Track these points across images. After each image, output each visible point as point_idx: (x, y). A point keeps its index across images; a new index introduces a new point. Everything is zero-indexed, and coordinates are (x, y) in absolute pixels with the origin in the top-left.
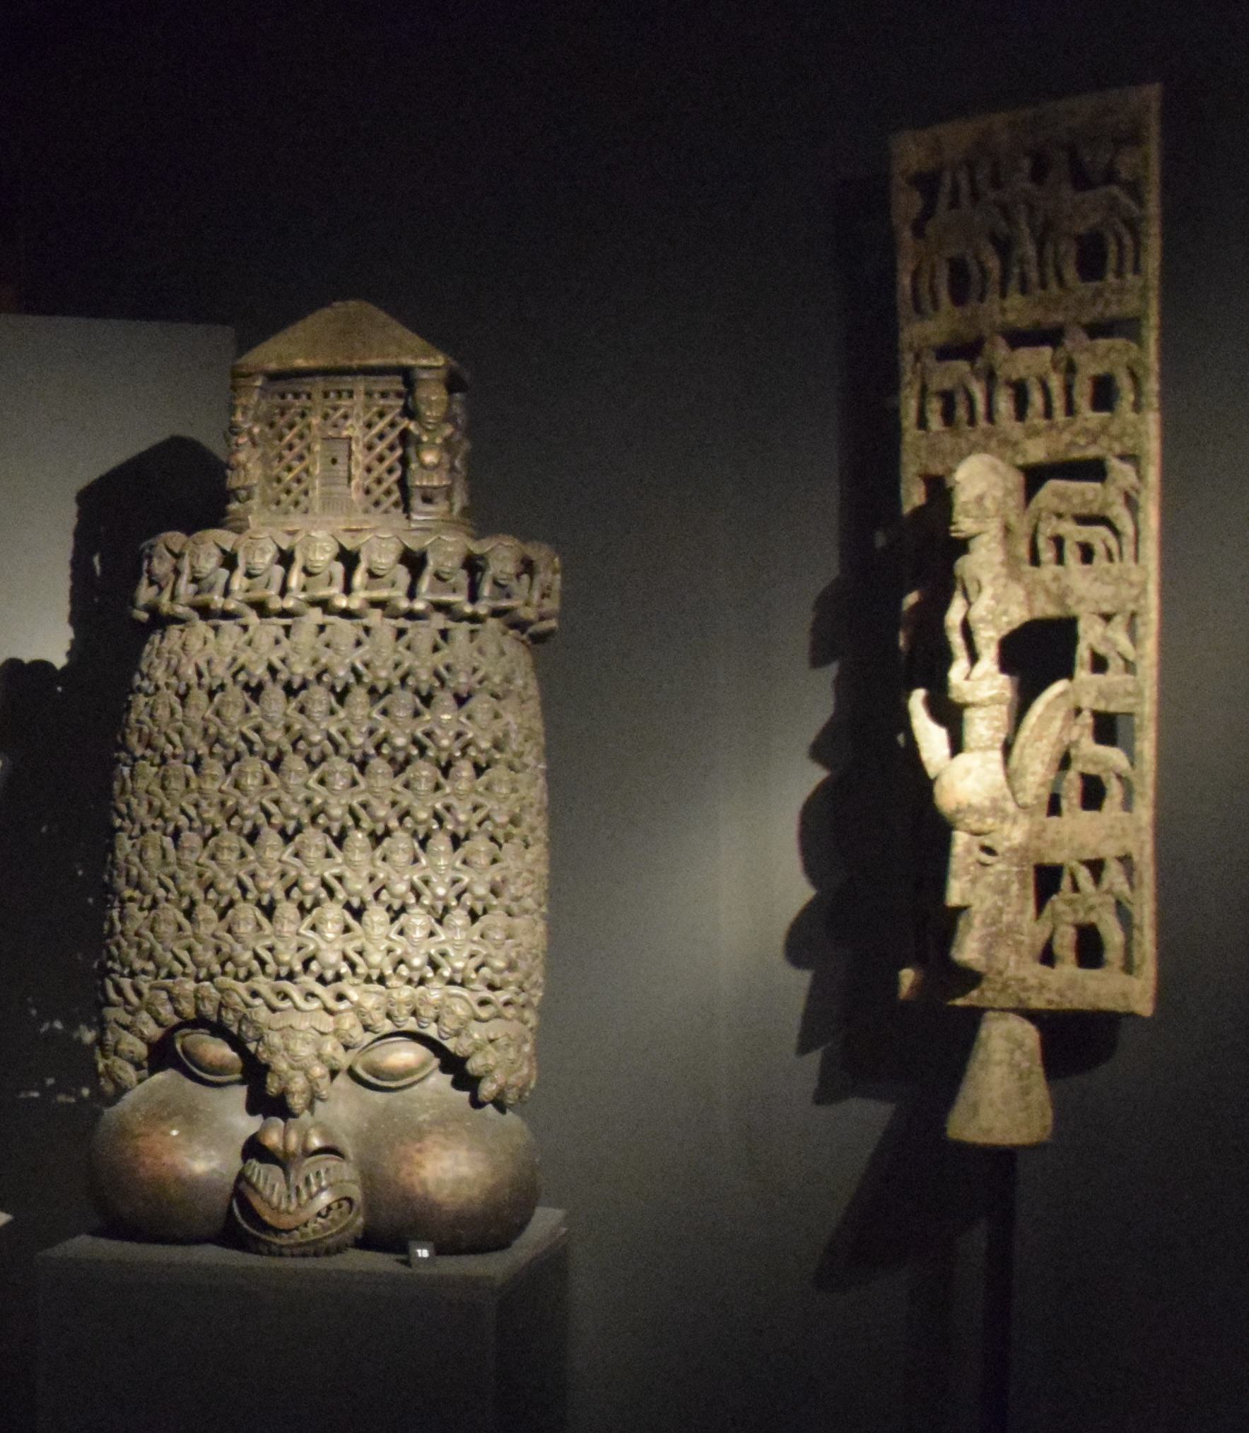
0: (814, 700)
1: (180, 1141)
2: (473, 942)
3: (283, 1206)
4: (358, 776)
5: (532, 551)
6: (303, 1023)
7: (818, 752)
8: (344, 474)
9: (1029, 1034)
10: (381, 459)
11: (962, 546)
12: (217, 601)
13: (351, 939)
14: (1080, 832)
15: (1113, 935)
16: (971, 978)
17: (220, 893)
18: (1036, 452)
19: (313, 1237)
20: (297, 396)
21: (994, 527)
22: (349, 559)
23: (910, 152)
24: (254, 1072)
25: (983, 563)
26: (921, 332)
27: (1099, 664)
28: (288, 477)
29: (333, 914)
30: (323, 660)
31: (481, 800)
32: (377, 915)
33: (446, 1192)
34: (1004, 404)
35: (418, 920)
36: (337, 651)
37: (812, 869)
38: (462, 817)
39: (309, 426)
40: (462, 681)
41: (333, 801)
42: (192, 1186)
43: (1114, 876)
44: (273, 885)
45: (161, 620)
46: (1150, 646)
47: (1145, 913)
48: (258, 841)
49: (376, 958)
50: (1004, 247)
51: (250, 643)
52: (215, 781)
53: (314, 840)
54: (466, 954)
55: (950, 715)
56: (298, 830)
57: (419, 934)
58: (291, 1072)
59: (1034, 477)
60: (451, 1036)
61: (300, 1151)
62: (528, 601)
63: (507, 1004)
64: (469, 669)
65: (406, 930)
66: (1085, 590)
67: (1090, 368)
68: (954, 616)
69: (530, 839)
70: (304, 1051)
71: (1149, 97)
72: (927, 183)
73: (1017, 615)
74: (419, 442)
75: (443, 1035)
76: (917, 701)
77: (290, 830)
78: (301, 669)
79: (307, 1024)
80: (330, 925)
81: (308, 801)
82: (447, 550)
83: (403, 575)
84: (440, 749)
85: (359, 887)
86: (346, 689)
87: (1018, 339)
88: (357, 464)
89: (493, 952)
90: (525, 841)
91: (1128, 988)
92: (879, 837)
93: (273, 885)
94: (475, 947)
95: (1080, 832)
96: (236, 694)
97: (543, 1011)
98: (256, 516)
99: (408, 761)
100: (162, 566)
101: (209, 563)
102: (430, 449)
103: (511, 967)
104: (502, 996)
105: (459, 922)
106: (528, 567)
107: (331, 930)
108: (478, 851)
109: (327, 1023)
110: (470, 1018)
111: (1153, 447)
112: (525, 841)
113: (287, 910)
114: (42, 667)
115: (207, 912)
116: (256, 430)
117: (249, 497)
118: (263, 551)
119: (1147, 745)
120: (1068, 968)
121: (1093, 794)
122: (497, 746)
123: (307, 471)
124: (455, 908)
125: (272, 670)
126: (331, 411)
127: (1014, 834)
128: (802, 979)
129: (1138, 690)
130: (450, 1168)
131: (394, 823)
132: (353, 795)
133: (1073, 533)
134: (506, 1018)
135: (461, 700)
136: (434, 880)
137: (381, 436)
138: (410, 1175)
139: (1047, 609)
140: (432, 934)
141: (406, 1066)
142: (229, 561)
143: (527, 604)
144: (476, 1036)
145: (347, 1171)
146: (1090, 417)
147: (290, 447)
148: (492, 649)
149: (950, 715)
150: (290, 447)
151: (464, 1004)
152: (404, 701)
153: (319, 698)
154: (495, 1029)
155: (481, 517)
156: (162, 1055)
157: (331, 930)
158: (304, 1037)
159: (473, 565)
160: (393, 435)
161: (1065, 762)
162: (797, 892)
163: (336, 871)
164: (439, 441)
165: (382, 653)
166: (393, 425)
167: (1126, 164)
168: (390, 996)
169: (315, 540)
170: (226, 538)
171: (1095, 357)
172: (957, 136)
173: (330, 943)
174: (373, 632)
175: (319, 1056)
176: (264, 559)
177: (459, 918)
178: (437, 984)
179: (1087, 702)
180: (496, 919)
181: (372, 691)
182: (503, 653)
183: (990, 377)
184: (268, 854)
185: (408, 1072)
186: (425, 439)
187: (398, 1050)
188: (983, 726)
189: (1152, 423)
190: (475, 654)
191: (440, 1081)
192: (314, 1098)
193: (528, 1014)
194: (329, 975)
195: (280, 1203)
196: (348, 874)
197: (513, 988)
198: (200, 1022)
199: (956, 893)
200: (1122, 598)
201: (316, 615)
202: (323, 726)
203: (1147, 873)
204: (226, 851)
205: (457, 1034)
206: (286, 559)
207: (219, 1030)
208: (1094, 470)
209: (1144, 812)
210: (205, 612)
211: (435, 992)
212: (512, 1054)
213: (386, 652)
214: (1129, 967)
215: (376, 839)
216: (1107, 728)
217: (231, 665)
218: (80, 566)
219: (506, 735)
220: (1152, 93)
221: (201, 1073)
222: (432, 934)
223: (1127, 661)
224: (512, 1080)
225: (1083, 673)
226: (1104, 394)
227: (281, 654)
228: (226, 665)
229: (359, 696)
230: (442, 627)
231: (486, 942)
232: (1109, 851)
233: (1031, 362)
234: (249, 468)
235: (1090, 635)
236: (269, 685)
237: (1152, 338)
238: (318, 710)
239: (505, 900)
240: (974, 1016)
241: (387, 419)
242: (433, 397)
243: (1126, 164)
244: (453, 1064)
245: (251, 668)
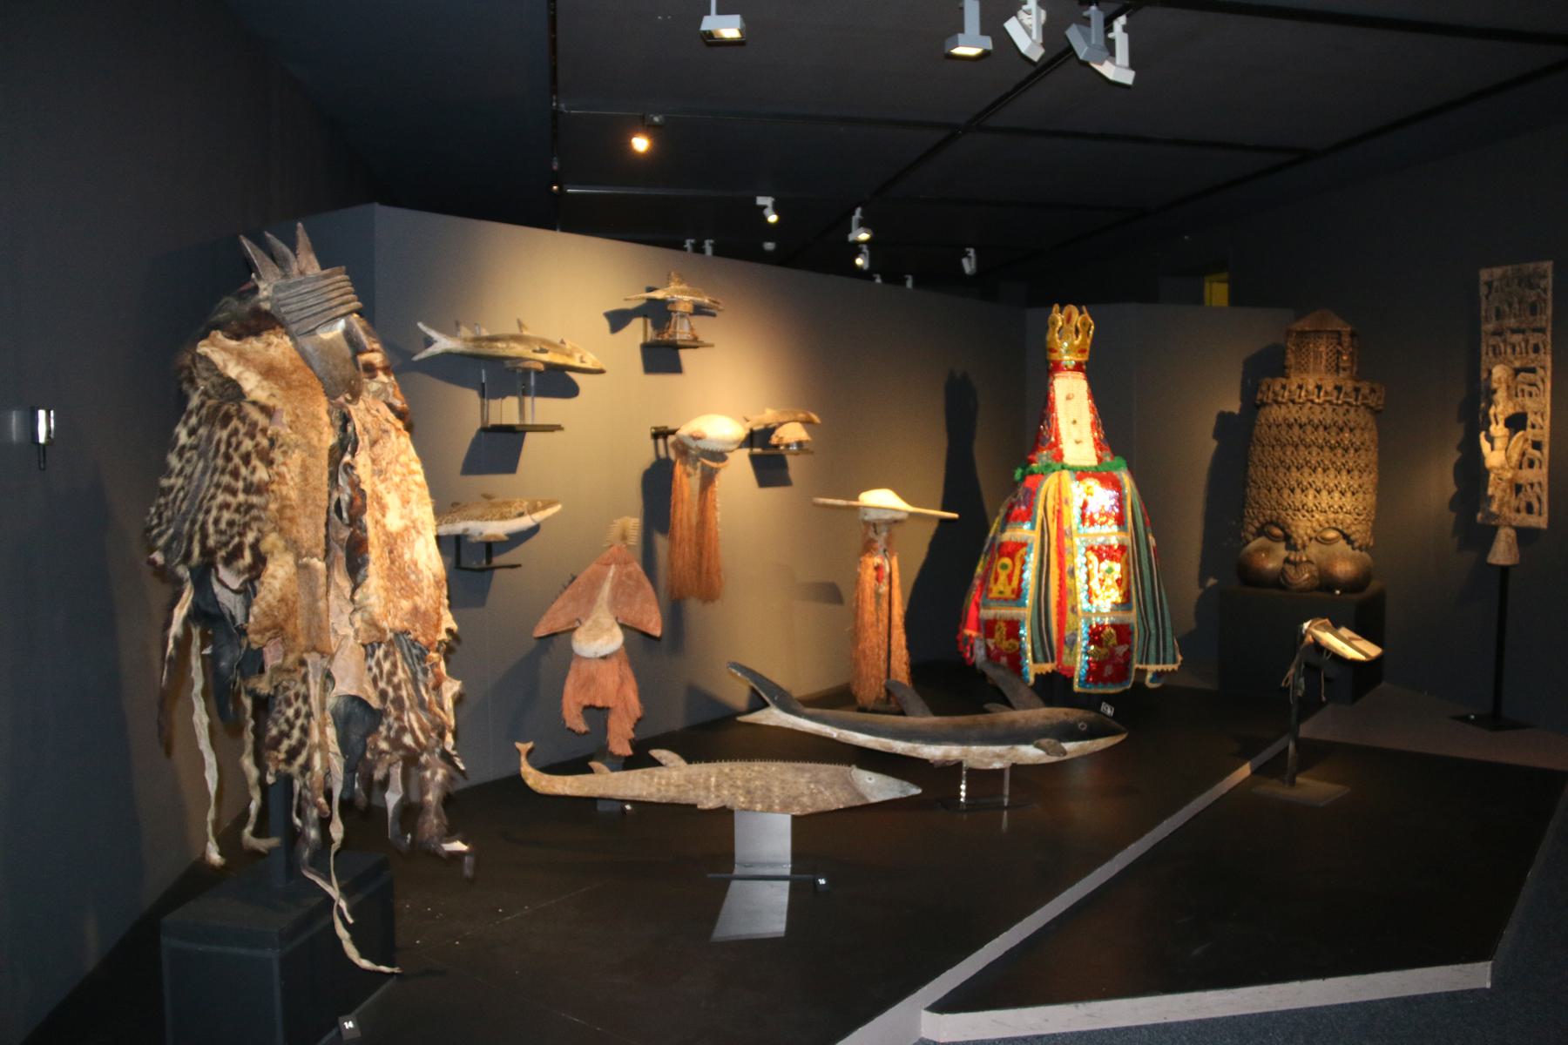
0: (1458, 433)
5: (1376, 386)
7: (1459, 448)
9: (1512, 533)
11: (1495, 392)
14: (1527, 475)
15: (1536, 505)
16: (1497, 517)
18: (1517, 364)
21: (1504, 386)
22: (1319, 388)
23: (1484, 275)
24: (1287, 538)
25: (1501, 396)
26: (1489, 327)
27: (1533, 426)
29: (1311, 493)
32: (1324, 493)
34: (1509, 350)
37: (1457, 483)
40: (1352, 424)
42: (1272, 571)
43: (1536, 488)
44: (1293, 483)
45: (1264, 404)
46: (1547, 422)
47: (1545, 499)
50: (1510, 305)
52: (1278, 452)
53: (1306, 470)
55: (1491, 439)
59: (1517, 372)
62: (1371, 401)
66: (1530, 404)
67: (1532, 342)
68: (1492, 411)
70: (1301, 532)
71: (1548, 266)
72: (1489, 284)
73: (1510, 411)
76: (1482, 435)
78: (1304, 420)
82: (1349, 386)
83: (1335, 393)
87: (1514, 331)
91: (1540, 521)
92: (1472, 471)
93: (1293, 483)
95: (1527, 475)
96: (1284, 427)
97: (1374, 522)
98: (1292, 373)
100: (1264, 388)
101: (1278, 388)
106: (1373, 391)
111: (1549, 365)
113: (1298, 491)
114: (1231, 414)
115: (1274, 491)
119: (1546, 450)
120: (1524, 514)
121: (1531, 464)
127: (1509, 475)
128: (1453, 515)
129: (1544, 435)
130: (1344, 568)
133: (1527, 388)
139: (1519, 410)
142: (1284, 387)
145: (1314, 568)
146: (1532, 356)
149: (1491, 439)
152: (1334, 431)
153: (1309, 429)
154: (1359, 527)
155: (1358, 377)
156: (1260, 532)
158: (1303, 527)
159: (1357, 390)
161: (1523, 454)
162: (1452, 489)
165: (1328, 416)
167: (1543, 284)
170: (1284, 381)
171: (1534, 339)
172: (1498, 272)
173: (1310, 500)
176: (1294, 387)
179: (1530, 437)
180: (1360, 495)
183: (1505, 341)
188: (1499, 444)
189: (1548, 359)
191: (1342, 542)
192: (1304, 547)
198: (1271, 523)
199: (1490, 491)
200: (1539, 407)
203: (1546, 487)
206: (1300, 387)
207: (1277, 525)
208: (1533, 371)
209: (1545, 470)
210: (1276, 402)
211: (1341, 516)
214: (1540, 514)
215: (1324, 471)
216: (1537, 445)
218: (1244, 383)
220: (1548, 266)
221: (1275, 538)
223: (1541, 425)
225: (1529, 429)
226: (1536, 349)
232: (1535, 481)
233: (1517, 338)
234: (1291, 359)
235: (1531, 418)
237: (1549, 334)
240: (1495, 529)
242: (1346, 340)
243: (1543, 284)
244: (1346, 537)
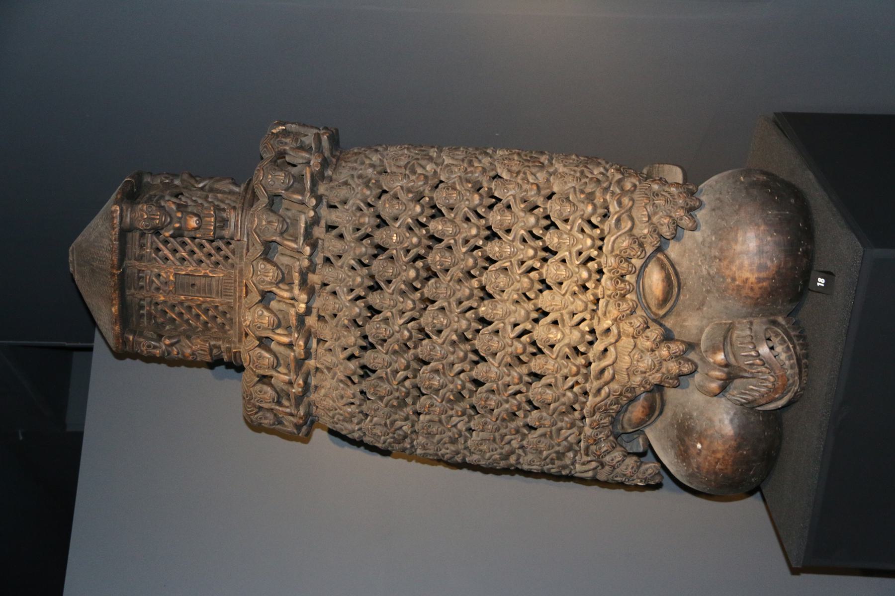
1: (706, 443)
2: (572, 228)
3: (770, 385)
4: (437, 305)
6: (625, 362)
8: (203, 280)
10: (192, 252)
12: (296, 390)
13: (563, 320)
17: (519, 409)
19: (795, 361)
20: (142, 307)
28: (203, 317)
30: (346, 322)
31: (461, 215)
32: (546, 300)
33: (769, 263)
35: (552, 271)
36: (340, 310)
38: (474, 231)
39: (165, 302)
40: (368, 220)
41: (455, 326)
48: (482, 380)
49: (579, 305)
51: (329, 369)
54: (581, 236)
56: (476, 352)
57: (563, 272)
58: (664, 370)
60: (644, 250)
61: (725, 369)
63: (620, 203)
64: (358, 214)
65: (559, 281)
69: (493, 174)
70: (647, 361)
74: (179, 229)
75: (642, 256)
77: (475, 358)
78: (352, 338)
79: (627, 358)
80: (551, 336)
81: (453, 343)
84: (419, 244)
85: (523, 312)
86: (370, 308)
88: (196, 270)
89: (579, 213)
90: (494, 178)
94: (576, 228)
99: (428, 268)
102: (186, 221)
103: (590, 198)
104: (614, 207)
105: (556, 240)
107: (555, 335)
108: (500, 220)
109: (626, 343)
110: (631, 235)
112: (494, 178)
113: (536, 365)
116: (168, 342)
117: (219, 347)
118: (260, 357)
122: (419, 199)
123: (199, 306)
124: (544, 242)
125: (351, 357)
126: (154, 286)
131: (475, 283)
132: (451, 312)
134: (631, 207)
135: (382, 223)
136: (521, 257)
137: (175, 251)
138: (752, 289)
140: (564, 261)
141: (663, 281)
143: (308, 163)
144: (646, 231)
147: (181, 314)
148: (343, 192)
150: (175, 251)
151: (620, 240)
153: (374, 328)
157: (555, 335)
160: (174, 243)
163: (509, 328)
164: (179, 215)
165: (343, 277)
166: (166, 242)
168: (609, 296)
169: (253, 321)
173: (565, 337)
174: (326, 282)
175: (653, 350)
177: (552, 239)
178: (603, 260)
181: (372, 289)
182: (346, 183)
184: (493, 375)
185: (668, 280)
186: (177, 225)
187: (650, 287)
190: (346, 207)
193: (628, 186)
194: (589, 338)
195: (766, 387)
196: (512, 320)
197: (608, 197)
201: (311, 321)
202: (397, 328)
204: (488, 403)
205: (641, 245)
211: (609, 262)
212: (660, 202)
213: (342, 275)
217: (348, 386)
219: (409, 191)
222: (564, 261)
224: (681, 202)
227: (339, 350)
228: (345, 387)
229: (375, 299)
230: (324, 230)
231: (571, 218)
236: (363, 361)
238: (384, 330)
239: (540, 201)
241: (161, 246)
245: (348, 373)
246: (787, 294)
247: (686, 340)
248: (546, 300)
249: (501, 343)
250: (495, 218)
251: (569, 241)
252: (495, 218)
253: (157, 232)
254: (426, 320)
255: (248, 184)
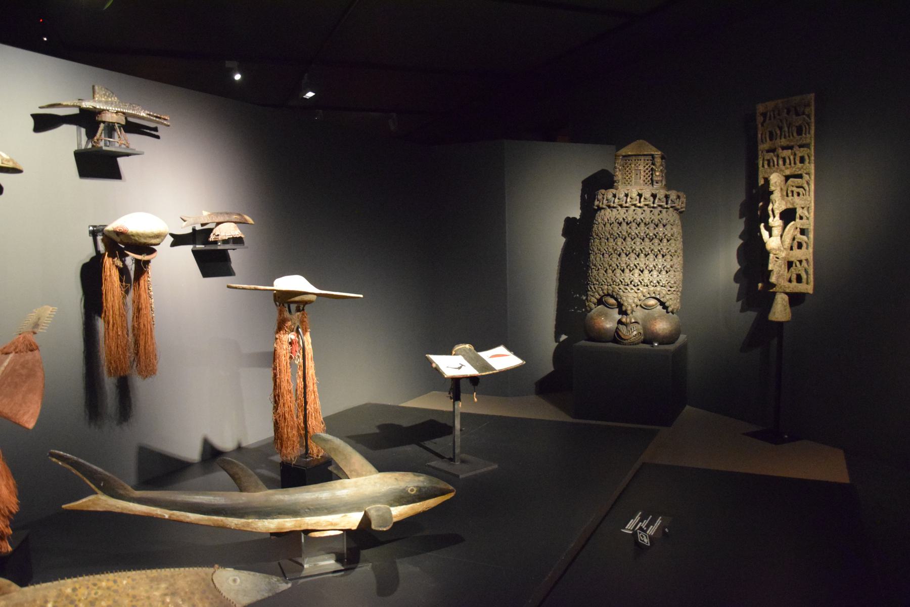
12: (612, 204)
35: (655, 273)
40: (664, 222)
70: (631, 301)
78: (630, 219)
107: (636, 275)
109: (636, 295)
153: (634, 225)
157: (636, 275)
165: (647, 216)
173: (636, 278)
177: (664, 272)
201: (633, 207)
211: (659, 288)
229: (642, 225)
246: (649, 338)
247: (788, 291)
248: (646, 272)
249: (633, 261)
250: (668, 257)
251: (663, 277)
252: (668, 257)
253: (653, 164)
254: (638, 239)
255: (132, 127)
